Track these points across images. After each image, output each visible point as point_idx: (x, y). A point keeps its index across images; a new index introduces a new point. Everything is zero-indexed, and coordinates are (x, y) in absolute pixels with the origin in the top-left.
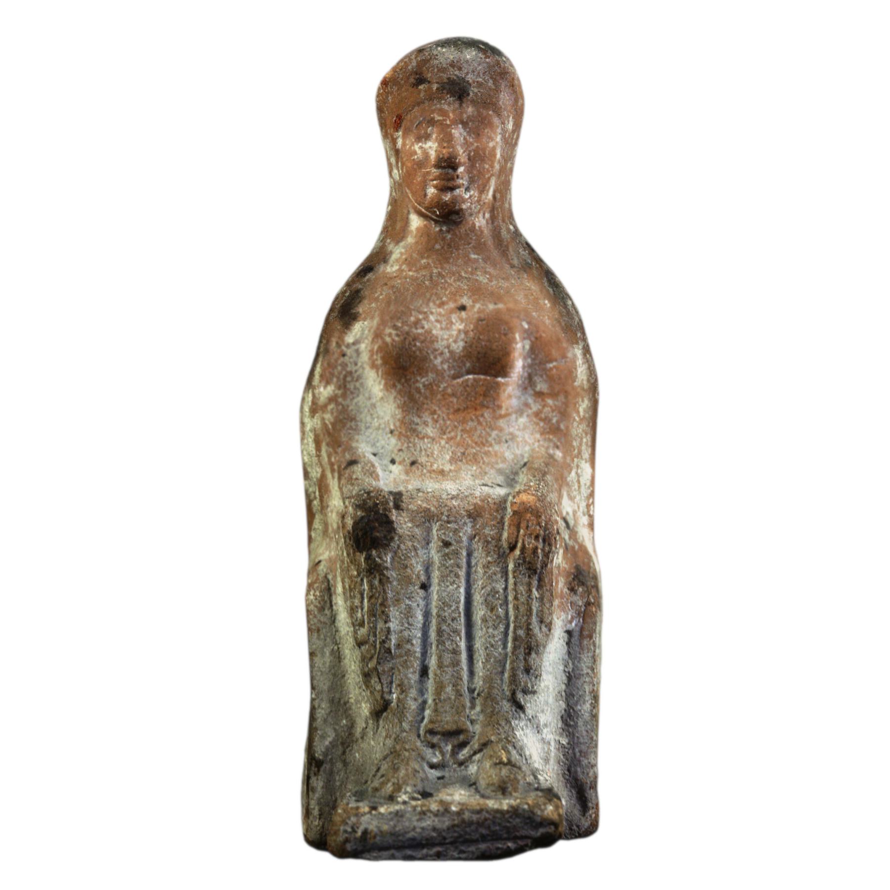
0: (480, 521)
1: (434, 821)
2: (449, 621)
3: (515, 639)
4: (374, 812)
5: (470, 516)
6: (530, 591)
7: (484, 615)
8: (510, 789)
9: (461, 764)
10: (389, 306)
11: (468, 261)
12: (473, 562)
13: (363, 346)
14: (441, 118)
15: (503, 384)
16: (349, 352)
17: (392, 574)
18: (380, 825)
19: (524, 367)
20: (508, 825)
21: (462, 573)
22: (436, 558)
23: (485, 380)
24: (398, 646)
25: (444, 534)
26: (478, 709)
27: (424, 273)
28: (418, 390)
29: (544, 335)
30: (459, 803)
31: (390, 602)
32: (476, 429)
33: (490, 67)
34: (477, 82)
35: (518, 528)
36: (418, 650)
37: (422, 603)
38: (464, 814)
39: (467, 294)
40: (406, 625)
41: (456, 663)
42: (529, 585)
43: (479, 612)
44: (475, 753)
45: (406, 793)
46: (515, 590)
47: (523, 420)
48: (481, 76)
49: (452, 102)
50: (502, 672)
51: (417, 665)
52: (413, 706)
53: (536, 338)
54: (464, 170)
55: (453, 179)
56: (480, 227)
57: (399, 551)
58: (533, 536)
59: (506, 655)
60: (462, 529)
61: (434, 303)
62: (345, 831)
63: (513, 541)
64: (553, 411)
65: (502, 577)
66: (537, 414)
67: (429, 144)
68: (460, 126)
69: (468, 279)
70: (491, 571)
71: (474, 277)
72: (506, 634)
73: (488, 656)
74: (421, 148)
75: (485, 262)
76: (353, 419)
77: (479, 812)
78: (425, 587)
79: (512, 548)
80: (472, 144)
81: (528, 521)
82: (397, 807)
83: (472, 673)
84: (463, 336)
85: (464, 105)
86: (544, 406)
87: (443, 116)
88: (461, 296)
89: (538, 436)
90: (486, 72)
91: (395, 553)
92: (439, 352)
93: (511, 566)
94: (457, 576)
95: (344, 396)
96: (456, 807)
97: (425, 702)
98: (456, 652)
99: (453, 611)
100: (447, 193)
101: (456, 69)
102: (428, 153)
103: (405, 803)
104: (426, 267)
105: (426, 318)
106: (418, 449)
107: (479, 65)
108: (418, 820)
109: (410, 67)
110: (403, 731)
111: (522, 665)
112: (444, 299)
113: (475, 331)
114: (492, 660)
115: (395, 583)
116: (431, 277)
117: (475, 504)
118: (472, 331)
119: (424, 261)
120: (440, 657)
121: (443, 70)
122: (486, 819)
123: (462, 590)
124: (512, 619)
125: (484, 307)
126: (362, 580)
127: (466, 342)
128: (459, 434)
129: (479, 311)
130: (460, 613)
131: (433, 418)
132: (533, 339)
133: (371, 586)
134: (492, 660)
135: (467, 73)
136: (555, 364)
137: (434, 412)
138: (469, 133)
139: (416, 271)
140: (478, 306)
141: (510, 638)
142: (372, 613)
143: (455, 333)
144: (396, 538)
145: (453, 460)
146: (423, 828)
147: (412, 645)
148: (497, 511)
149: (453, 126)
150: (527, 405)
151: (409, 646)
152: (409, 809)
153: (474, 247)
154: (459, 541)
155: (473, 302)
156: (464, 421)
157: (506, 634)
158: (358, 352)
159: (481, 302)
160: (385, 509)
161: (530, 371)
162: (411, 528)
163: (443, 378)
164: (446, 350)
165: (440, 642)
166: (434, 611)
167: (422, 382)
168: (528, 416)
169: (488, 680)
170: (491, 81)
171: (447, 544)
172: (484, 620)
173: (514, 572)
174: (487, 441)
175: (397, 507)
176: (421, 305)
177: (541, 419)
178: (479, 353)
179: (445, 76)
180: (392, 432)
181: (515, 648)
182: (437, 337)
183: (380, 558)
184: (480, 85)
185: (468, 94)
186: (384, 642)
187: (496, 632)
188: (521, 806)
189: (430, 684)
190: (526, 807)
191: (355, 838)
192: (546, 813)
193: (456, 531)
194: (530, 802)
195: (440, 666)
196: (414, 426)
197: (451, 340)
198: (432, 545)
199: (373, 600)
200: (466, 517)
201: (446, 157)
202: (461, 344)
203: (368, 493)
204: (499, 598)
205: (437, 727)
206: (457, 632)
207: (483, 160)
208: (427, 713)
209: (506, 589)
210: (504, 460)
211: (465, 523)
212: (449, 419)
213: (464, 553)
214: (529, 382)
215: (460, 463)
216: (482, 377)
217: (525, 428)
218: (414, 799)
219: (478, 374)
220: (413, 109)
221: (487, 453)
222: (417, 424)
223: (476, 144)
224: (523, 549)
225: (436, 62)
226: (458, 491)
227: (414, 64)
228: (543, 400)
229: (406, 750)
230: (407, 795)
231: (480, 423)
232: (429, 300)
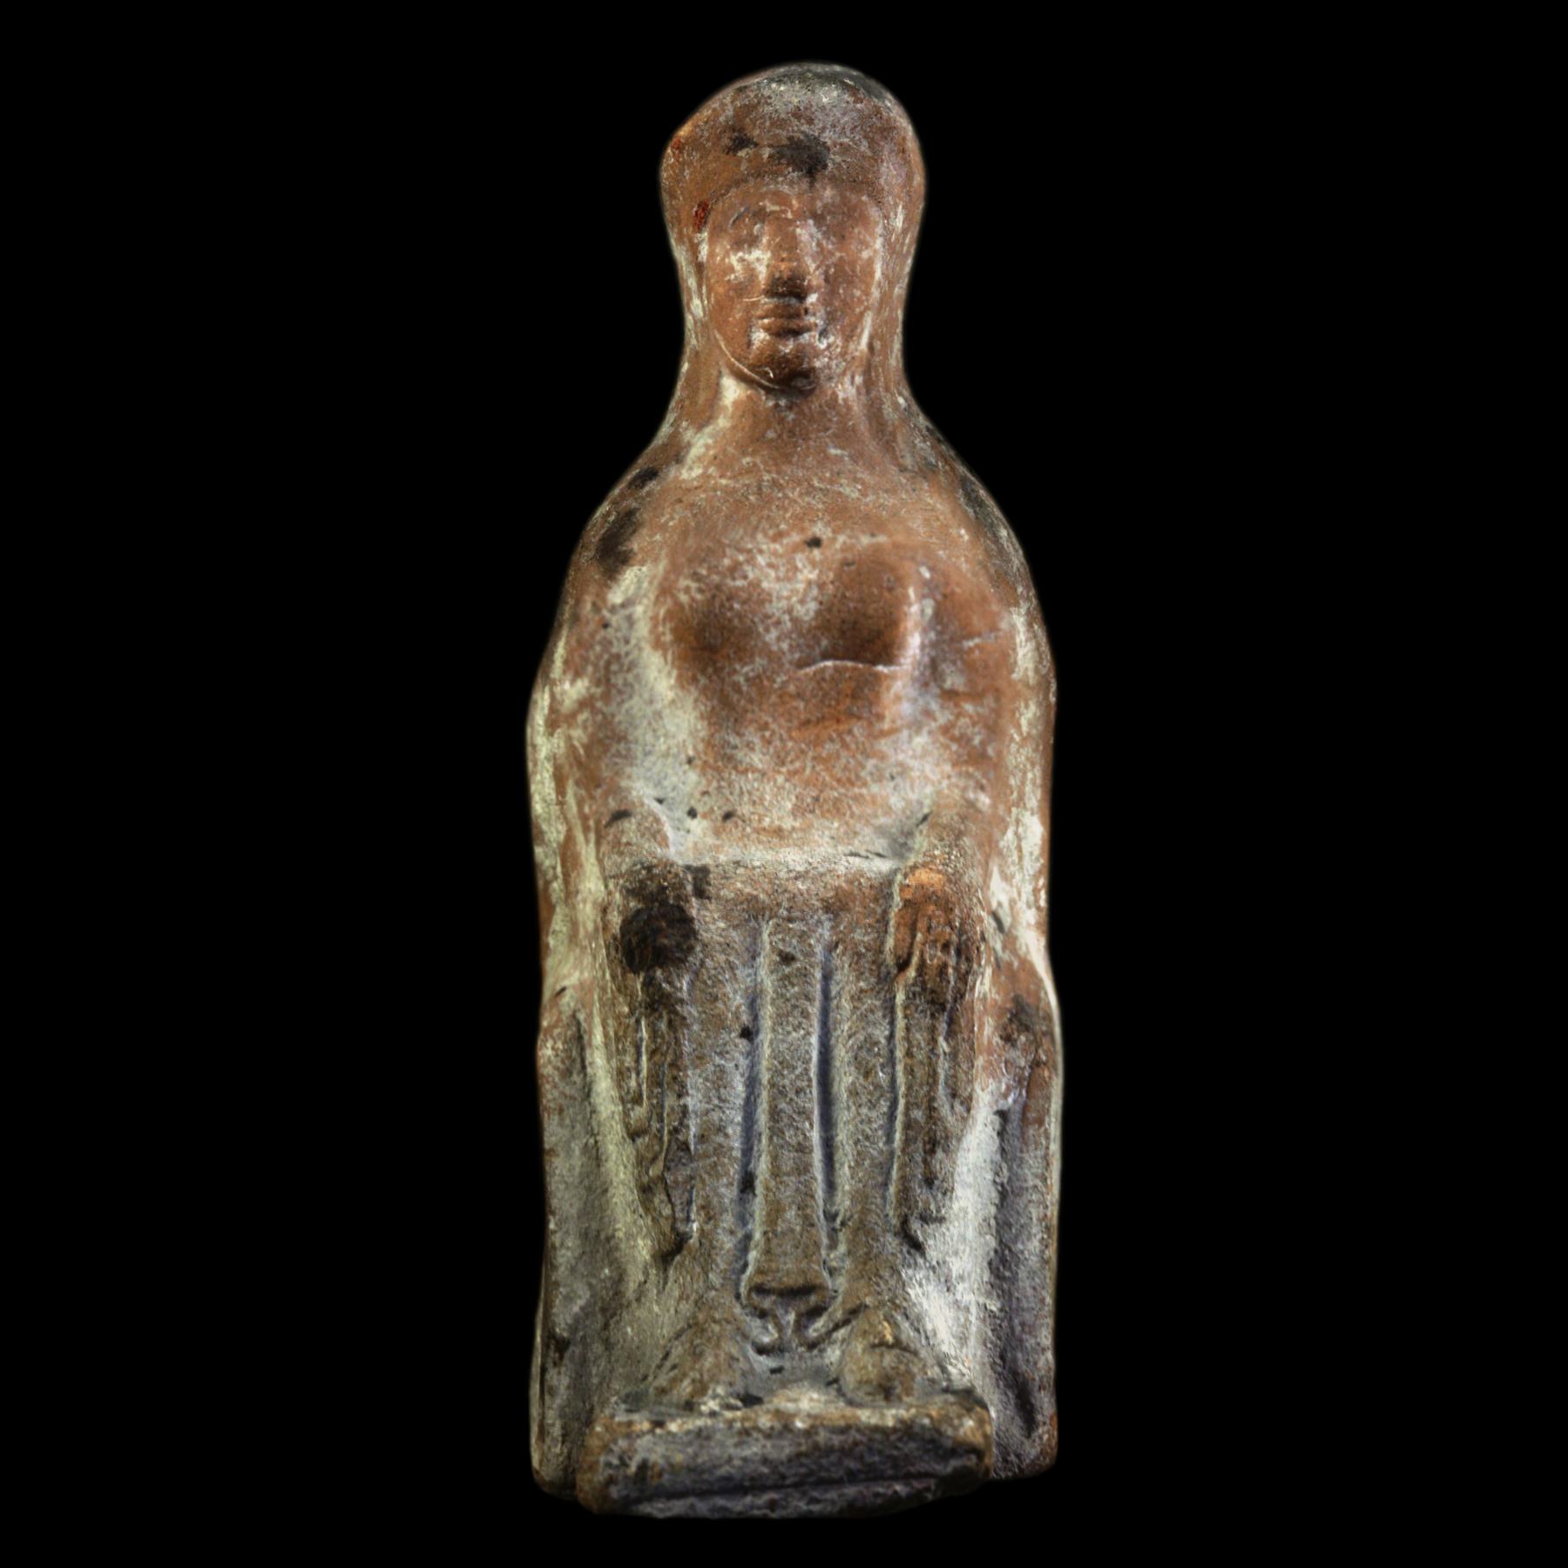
0: (846, 918)
1: (764, 1446)
2: (792, 1095)
3: (908, 1125)
4: (658, 1431)
5: (827, 908)
7: (853, 1083)
8: (898, 1391)
9: (812, 1346)
10: (685, 539)
11: (825, 459)
12: (834, 990)
13: (639, 610)
14: (776, 208)
15: (886, 676)
16: (615, 620)
17: (691, 1011)
19: (923, 647)
20: (895, 1453)
21: (814, 1010)
22: (768, 982)
23: (855, 669)
24: (702, 1138)
25: (783, 940)
26: (842, 1248)
28: (737, 688)
29: (958, 590)
30: (809, 1416)
31: (686, 1061)
32: (838, 757)
33: (863, 118)
34: (841, 144)
35: (913, 930)
36: (736, 1145)
37: (744, 1062)
38: (817, 1433)
39: (822, 519)
40: (716, 1102)
41: (803, 1169)
42: (933, 1030)
43: (845, 1079)
44: (837, 1327)
45: (715, 1397)
46: (907, 1039)
47: (921, 740)
48: (848, 133)
49: (795, 180)
50: (885, 1185)
51: (734, 1171)
52: (728, 1243)
53: (945, 596)
54: (818, 300)
55: (798, 315)
56: (845, 400)
57: (704, 971)
59: (892, 1153)
60: (814, 932)
61: (765, 534)
62: (609, 1465)
63: (903, 952)
64: (974, 724)
65: (884, 1016)
66: (946, 730)
67: (756, 254)
68: (811, 222)
69: (825, 492)
70: (866, 1006)
71: (836, 488)
72: (891, 1117)
73: (860, 1157)
74: (742, 260)
75: (855, 462)
76: (622, 738)
77: (844, 1430)
78: (748, 1034)
79: (903, 965)
80: (832, 254)
81: (930, 919)
82: (700, 1422)
83: (831, 1186)
84: (815, 592)
85: (818, 185)
86: (958, 716)
87: (780, 204)
88: (813, 522)
89: (948, 768)
90: (856, 127)
91: (697, 974)
92: (774, 619)
93: (900, 998)
94: (805, 1015)
95: (606, 697)
96: (804, 1422)
97: (748, 1237)
98: (803, 1149)
99: (797, 1077)
100: (788, 340)
101: (803, 121)
102: (753, 270)
103: (713, 1414)
104: (751, 470)
105: (751, 561)
106: (737, 791)
107: (844, 114)
108: (736, 1445)
109: (722, 119)
110: (711, 1287)
112: (783, 526)
113: (837, 584)
114: (867, 1163)
115: (696, 1027)
116: (760, 488)
117: (837, 889)
118: (832, 582)
119: (746, 460)
120: (775, 1158)
121: (780, 123)
122: (856, 1444)
123: (814, 1040)
124: (902, 1090)
125: (854, 541)
126: (638, 1022)
127: (821, 603)
128: (809, 764)
129: (845, 549)
130: (810, 1080)
131: (763, 737)
132: (939, 597)
133: (654, 1033)
134: (867, 1163)
135: (823, 129)
136: (977, 640)
138: (826, 235)
139: (733, 477)
140: (841, 539)
141: (899, 1125)
142: (656, 1080)
143: (801, 586)
144: (698, 948)
145: (797, 811)
146: (745, 1460)
147: (726, 1136)
148: (876, 900)
149: (798, 223)
150: (928, 713)
151: (720, 1139)
152: (721, 1425)
153: (836, 436)
154: (809, 954)
155: (834, 532)
156: (817, 743)
157: (891, 1117)
158: (630, 620)
159: (848, 532)
160: (678, 897)
161: (933, 653)
162: (723, 930)
164: (787, 617)
165: (776, 1132)
166: (765, 1077)
167: (743, 672)
168: (930, 733)
169: (861, 1197)
170: (865, 143)
171: (787, 959)
172: (853, 1092)
173: (906, 1008)
174: (858, 777)
175: (700, 893)
176: (742, 538)
177: (953, 739)
179: (783, 134)
180: (690, 761)
181: (907, 1142)
182: (770, 595)
183: (670, 983)
184: (845, 149)
185: (825, 166)
186: (676, 1131)
188: (917, 1420)
189: (758, 1205)
190: (926, 1421)
191: (626, 1477)
192: (961, 1431)
193: (803, 936)
194: (934, 1413)
195: (776, 1173)
196: (729, 751)
197: (794, 599)
198: (760, 960)
199: (657, 1058)
200: (820, 911)
201: (785, 277)
202: (813, 606)
204: (878, 1054)
206: (804, 1113)
208: (753, 1255)
209: (891, 1037)
210: (888, 810)
211: (819, 922)
212: (791, 738)
213: (818, 975)
214: (932, 672)
216: (850, 664)
217: (925, 754)
218: (730, 1407)
219: (842, 658)
220: (728, 192)
221: (858, 799)
222: (735, 747)
223: (838, 254)
224: (922, 967)
225: (768, 109)
226: (806, 865)
227: (730, 112)
228: (957, 705)
229: (715, 1321)
230: (717, 1401)
231: (845, 745)
232: (756, 528)
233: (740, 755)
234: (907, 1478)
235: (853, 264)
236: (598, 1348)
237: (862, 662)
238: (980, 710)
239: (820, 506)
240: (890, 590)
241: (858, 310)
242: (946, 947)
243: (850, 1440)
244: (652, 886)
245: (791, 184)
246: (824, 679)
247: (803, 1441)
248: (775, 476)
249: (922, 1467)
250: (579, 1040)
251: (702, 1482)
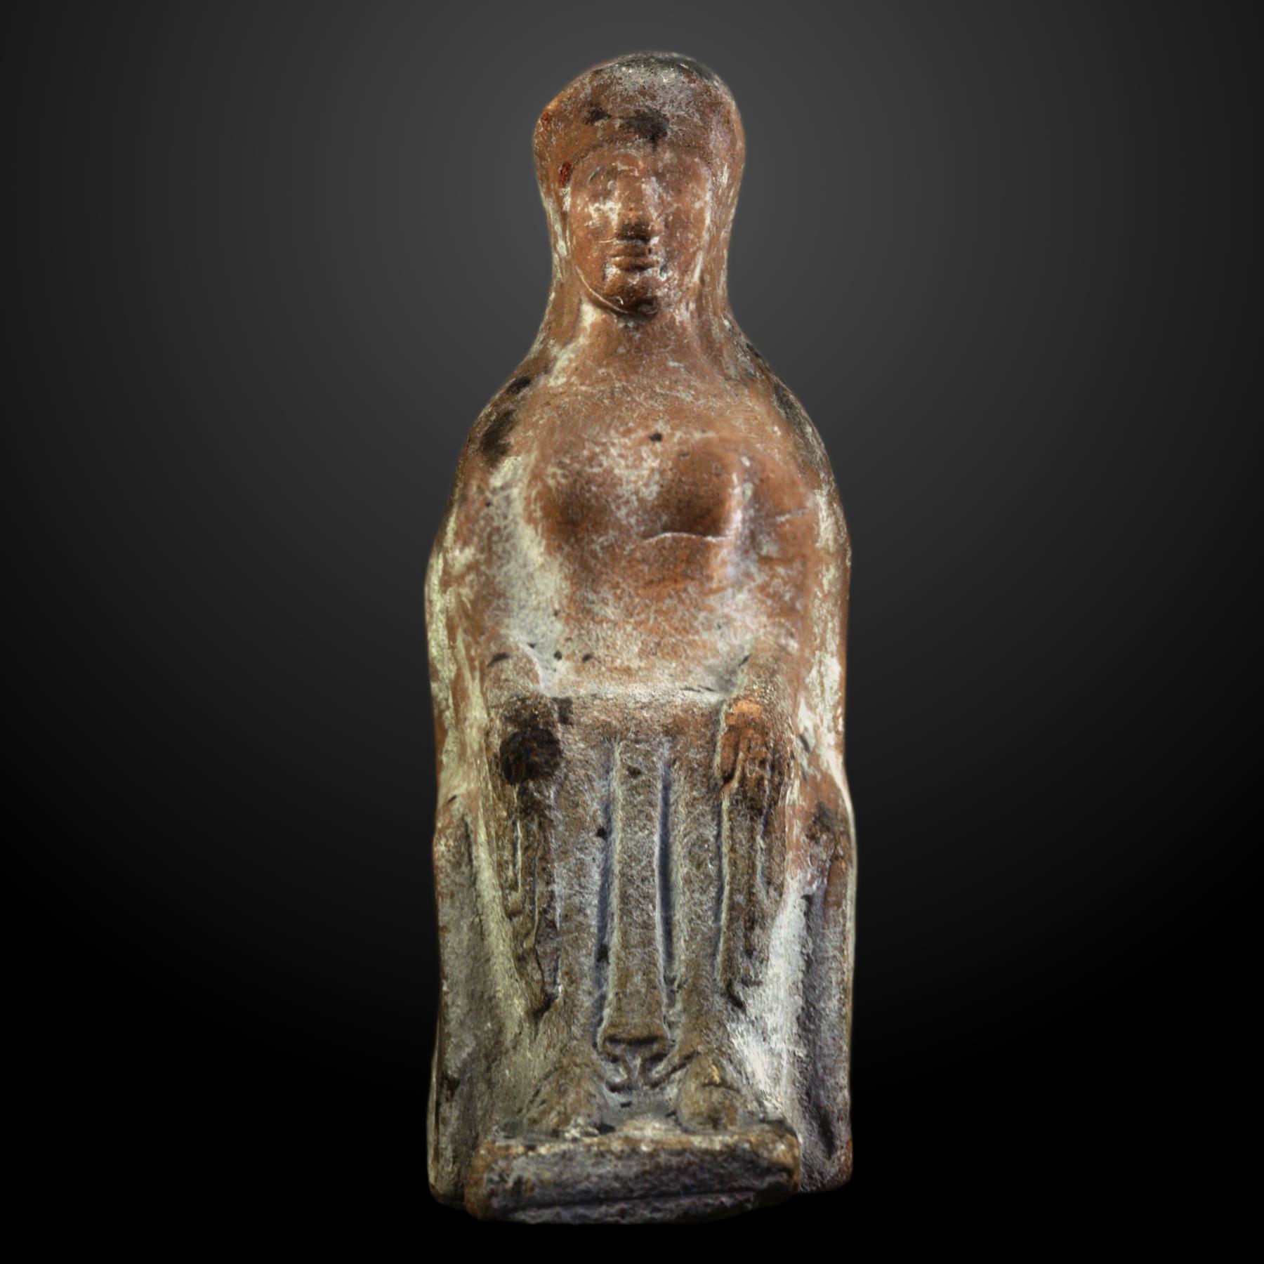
0: (682, 740)
1: (616, 1166)
2: (638, 882)
3: (732, 907)
4: (531, 1153)
5: (667, 732)
6: (753, 839)
8: (724, 1121)
9: (655, 1085)
10: (552, 435)
11: (665, 370)
12: (672, 798)
13: (515, 492)
14: (626, 168)
15: (715, 545)
16: (495, 500)
17: (557, 815)
18: (539, 1172)
19: (744, 521)
20: (722, 1171)
21: (657, 814)
22: (619, 792)
23: (689, 539)
24: (566, 918)
25: (631, 758)
26: (679, 1006)
27: (602, 388)
28: (594, 555)
29: (772, 476)
30: (652, 1141)
31: (553, 855)
32: (676, 610)
33: (696, 95)
34: (678, 116)
35: (736, 750)
36: (594, 923)
37: (599, 856)
38: (658, 1155)
39: (663, 418)
40: (577, 888)
41: (648, 942)
42: (752, 830)
43: (681, 870)
44: (674, 1070)
45: (576, 1126)
46: (731, 838)
47: (743, 597)
49: (641, 145)
50: (714, 955)
51: (592, 944)
52: (587, 1002)
53: (762, 480)
54: (659, 241)
55: (643, 254)
56: (681, 323)
57: (567, 782)
59: (719, 930)
60: (656, 751)
61: (617, 431)
62: (491, 1181)
63: (728, 768)
64: (785, 584)
65: (713, 819)
66: (762, 588)
67: (610, 204)
68: (654, 179)
69: (665, 397)
70: (698, 811)
71: (674, 393)
72: (718, 900)
73: (693, 932)
74: (598, 210)
75: (689, 372)
76: (501, 595)
77: (680, 1153)
78: (603, 833)
79: (728, 778)
80: (671, 205)
81: (750, 740)
82: (564, 1147)
83: (670, 956)
84: (657, 477)
85: (659, 149)
86: (772, 577)
87: (629, 165)
88: (655, 420)
89: (764, 619)
90: (690, 102)
91: (562, 785)
92: (624, 499)
93: (726, 804)
94: (649, 818)
95: (489, 562)
96: (648, 1146)
97: (603, 997)
98: (647, 926)
99: (643, 868)
100: (635, 274)
102: (607, 217)
103: (575, 1140)
104: (606, 379)
105: (605, 452)
106: (594, 637)
107: (680, 92)
108: (594, 1165)
109: (582, 96)
110: (573, 1038)
111: (741, 945)
112: (631, 424)
113: (674, 471)
114: (699, 937)
115: (561, 828)
116: (612, 394)
117: (675, 716)
118: (671, 470)
119: (602, 371)
120: (625, 934)
121: (629, 99)
122: (690, 1164)
123: (656, 838)
124: (727, 878)
126: (514, 824)
127: (662, 486)
128: (652, 616)
129: (681, 442)
130: (653, 871)
131: (615, 594)
132: (757, 481)
133: (527, 833)
134: (699, 937)
135: (664, 104)
136: (788, 516)
137: (617, 586)
138: (666, 189)
139: (591, 385)
140: (678, 434)
141: (724, 907)
142: (529, 871)
143: (646, 473)
144: (563, 765)
145: (643, 654)
146: (600, 1177)
147: (586, 915)
148: (706, 726)
149: (643, 180)
150: (748, 575)
151: (580, 918)
152: (582, 1149)
153: (674, 351)
154: (652, 769)
155: (672, 429)
156: (659, 599)
157: (718, 900)
158: (508, 500)
160: (547, 723)
161: (752, 527)
162: (583, 749)
163: (630, 537)
164: (634, 498)
165: (625, 912)
166: (617, 868)
167: (599, 542)
168: (750, 591)
169: (694, 965)
170: (697, 115)
171: (634, 773)
172: (688, 881)
173: (730, 812)
175: (565, 720)
176: (598, 434)
177: (768, 596)
179: (631, 108)
180: (556, 613)
181: (731, 920)
182: (620, 479)
183: (540, 792)
184: (681, 120)
185: (665, 134)
186: (545, 911)
187: (704, 898)
188: (740, 1145)
189: (611, 972)
190: (747, 1146)
191: (505, 1191)
192: (775, 1154)
193: (647, 755)
194: (753, 1139)
195: (625, 945)
196: (587, 606)
197: (640, 483)
198: (613, 774)
199: (529, 852)
200: (661, 735)
201: (633, 223)
202: (655, 488)
204: (708, 850)
206: (648, 897)
208: (607, 1012)
209: (718, 836)
210: (716, 653)
211: (661, 743)
212: (638, 595)
213: (660, 786)
214: (751, 542)
216: (685, 535)
217: (745, 608)
218: (588, 1134)
219: (679, 531)
220: (586, 154)
221: (692, 644)
222: (593, 602)
223: (675, 205)
224: (743, 779)
225: (619, 88)
227: (588, 90)
228: (771, 568)
229: (576, 1065)
230: (578, 1129)
231: (681, 601)
232: (609, 426)
233: (596, 608)
234: (731, 1191)
235: (687, 213)
236: (482, 1086)
237: (695, 534)
238: (790, 572)
240: (718, 475)
243: (685, 1161)
244: (525, 714)
245: (638, 148)
246: (664, 548)
247: (647, 1161)
248: (624, 383)
250: (467, 838)
251: (566, 1195)
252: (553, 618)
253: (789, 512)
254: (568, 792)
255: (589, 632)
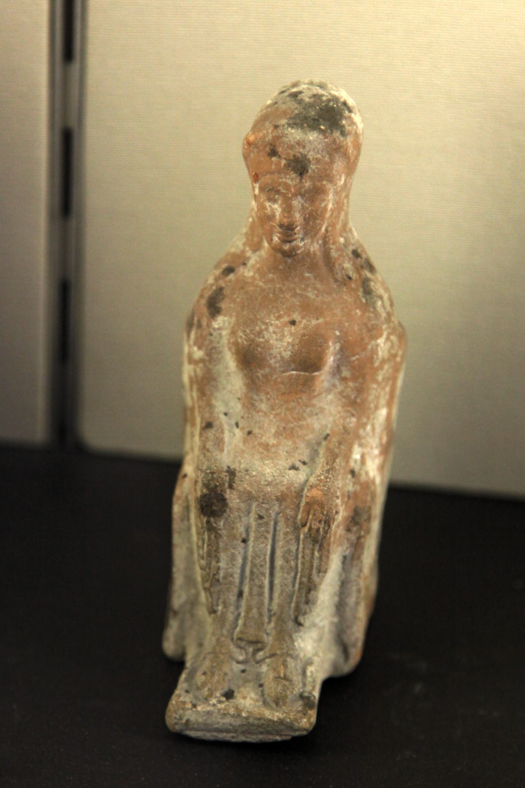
0: (284, 504)
1: (231, 720)
2: (259, 567)
3: (301, 583)
4: (194, 709)
5: (277, 500)
6: (313, 554)
7: (282, 565)
8: (281, 704)
9: (258, 662)
10: (243, 310)
11: (303, 279)
12: (278, 528)
13: (224, 333)
14: (284, 191)
15: (317, 376)
16: (215, 334)
17: (224, 532)
18: (196, 718)
19: (334, 361)
20: (276, 728)
21: (270, 536)
22: (253, 524)
23: (304, 375)
24: (225, 578)
25: (260, 510)
26: (272, 625)
27: (270, 286)
28: (258, 378)
29: (351, 338)
30: (248, 711)
31: (221, 550)
32: (295, 408)
33: (328, 145)
34: (316, 159)
35: (308, 514)
36: (237, 581)
37: (242, 551)
38: (249, 719)
39: (298, 310)
40: (231, 565)
41: (261, 594)
42: (313, 550)
43: (279, 562)
44: (267, 658)
45: (216, 697)
46: (303, 552)
47: (330, 397)
48: (320, 152)
49: (294, 177)
50: (290, 603)
51: (236, 590)
52: (231, 617)
53: (345, 341)
54: (300, 228)
55: (291, 235)
56: (314, 252)
57: (229, 518)
58: (318, 520)
59: (294, 591)
60: (272, 508)
61: (274, 315)
62: (176, 718)
63: (304, 522)
64: (352, 390)
65: (295, 542)
66: (341, 393)
67: (276, 206)
68: (299, 197)
69: (301, 295)
70: (289, 538)
71: (305, 293)
72: (295, 578)
73: (282, 591)
74: (270, 206)
75: (316, 279)
76: (215, 380)
77: (259, 719)
78: (244, 541)
79: (304, 525)
80: (307, 208)
81: (315, 511)
82: (209, 708)
83: (271, 598)
84: (290, 347)
85: (304, 180)
86: (346, 387)
87: (286, 190)
88: (294, 312)
89: (340, 408)
90: (324, 149)
91: (227, 519)
92: (274, 355)
93: (302, 536)
94: (266, 538)
95: (210, 361)
96: (245, 714)
97: (239, 615)
98: (261, 587)
99: (261, 561)
100: (287, 244)
101: (301, 147)
102: (274, 212)
103: (214, 705)
104: (272, 281)
105: (267, 329)
106: (254, 421)
107: (319, 144)
108: (221, 718)
109: (267, 139)
110: (222, 635)
111: (303, 600)
112: (282, 313)
113: (299, 345)
114: (285, 594)
115: (225, 538)
116: (274, 291)
117: (282, 492)
118: (297, 344)
119: (271, 276)
120: (251, 589)
121: (291, 147)
122: (263, 724)
123: (269, 547)
124: (300, 570)
125: (308, 323)
126: (204, 532)
127: (292, 353)
128: (284, 411)
129: (305, 328)
130: (266, 562)
131: (267, 398)
132: (342, 342)
133: (209, 539)
134: (285, 594)
135: (309, 151)
136: (357, 357)
137: (267, 393)
138: (306, 201)
139: (265, 283)
140: (304, 321)
141: (298, 581)
142: (209, 554)
143: (285, 344)
144: (228, 510)
145: (277, 434)
146: (224, 724)
147: (234, 578)
148: (296, 498)
149: (293, 198)
150: (334, 386)
151: (231, 579)
152: (216, 711)
153: (308, 268)
154: (270, 516)
155: (302, 318)
156: (287, 402)
157: (295, 578)
158: (220, 336)
159: (307, 318)
160: (222, 491)
161: (339, 363)
162: (238, 503)
163: (275, 372)
164: (278, 355)
165: (252, 579)
166: (250, 558)
167: (260, 373)
168: (335, 394)
169: (281, 607)
170: (327, 156)
171: (261, 517)
172: (282, 568)
173: (303, 541)
174: (302, 416)
175: (231, 487)
176: (264, 316)
177: (344, 397)
178: (300, 360)
179: (292, 153)
180: (239, 399)
181: (300, 589)
182: (273, 346)
183: (216, 523)
184: (318, 161)
185: (307, 172)
186: (214, 575)
187: (288, 577)
188: (285, 720)
189: (243, 603)
190: (288, 720)
191: (182, 724)
192: (301, 724)
193: (267, 510)
194: (291, 717)
195: (251, 594)
196: (253, 402)
197: (282, 349)
198: (251, 514)
199: (210, 547)
200: (275, 501)
201: (285, 225)
202: (289, 353)
203: (212, 473)
204: (292, 556)
205: (243, 636)
206: (263, 574)
207: (315, 219)
208: (240, 622)
209: (297, 550)
210: (313, 431)
211: (274, 505)
212: (278, 399)
213: (272, 523)
214: (337, 370)
215: (281, 437)
216: (302, 373)
217: (332, 402)
218: (220, 702)
219: (299, 371)
220: (266, 175)
221: (301, 427)
222: (256, 400)
223: (310, 208)
224: (310, 529)
225: (287, 139)
226: (272, 478)
227: (270, 137)
228: (346, 383)
229: (223, 654)
230: (216, 699)
231: (299, 403)
232: (271, 311)
233: (257, 404)
234: (281, 735)
235: (316, 211)
236: (188, 616)
237: (308, 372)
238: (356, 385)
239: (298, 303)
240: (321, 346)
241: (318, 228)
242: (320, 522)
243: (261, 723)
244: (212, 485)
245: (292, 179)
246: (292, 378)
247: (244, 720)
248: (281, 286)
249: (287, 733)
250: (187, 508)
251: (207, 728)
252: (237, 400)
253: (358, 354)
254: (229, 522)
255: (252, 417)
